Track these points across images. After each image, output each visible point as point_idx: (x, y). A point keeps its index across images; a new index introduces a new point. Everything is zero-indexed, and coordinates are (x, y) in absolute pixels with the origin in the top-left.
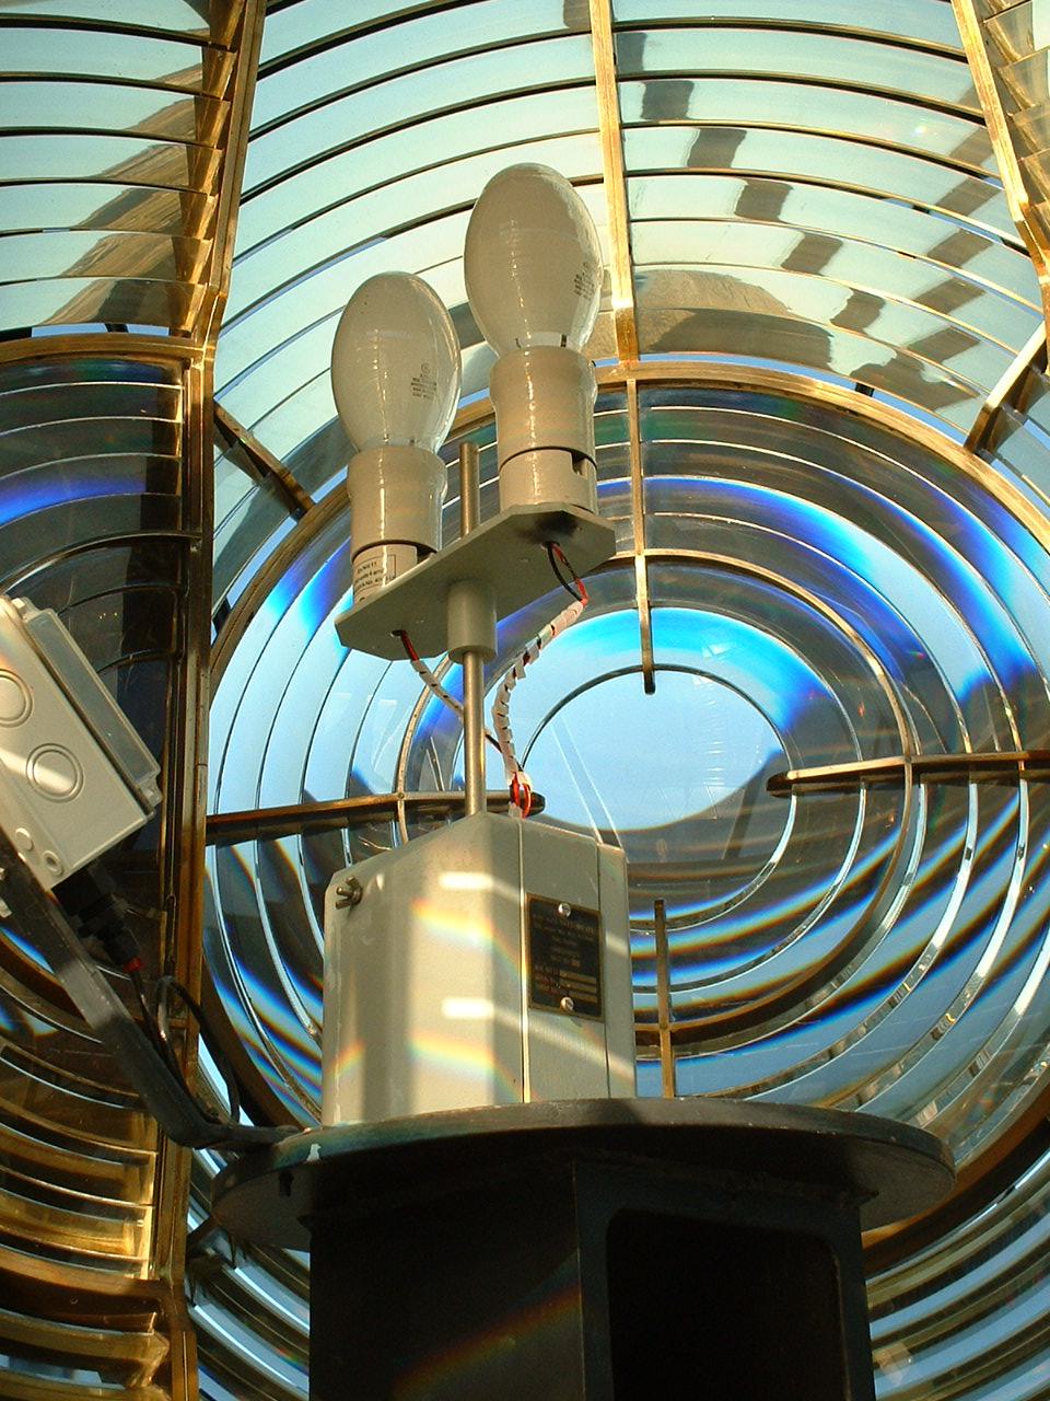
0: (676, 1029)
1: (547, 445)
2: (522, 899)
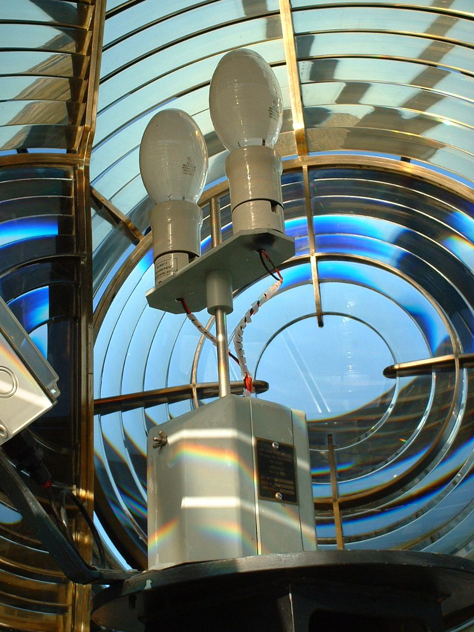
0: (341, 501)
1: (259, 198)
2: (253, 442)
